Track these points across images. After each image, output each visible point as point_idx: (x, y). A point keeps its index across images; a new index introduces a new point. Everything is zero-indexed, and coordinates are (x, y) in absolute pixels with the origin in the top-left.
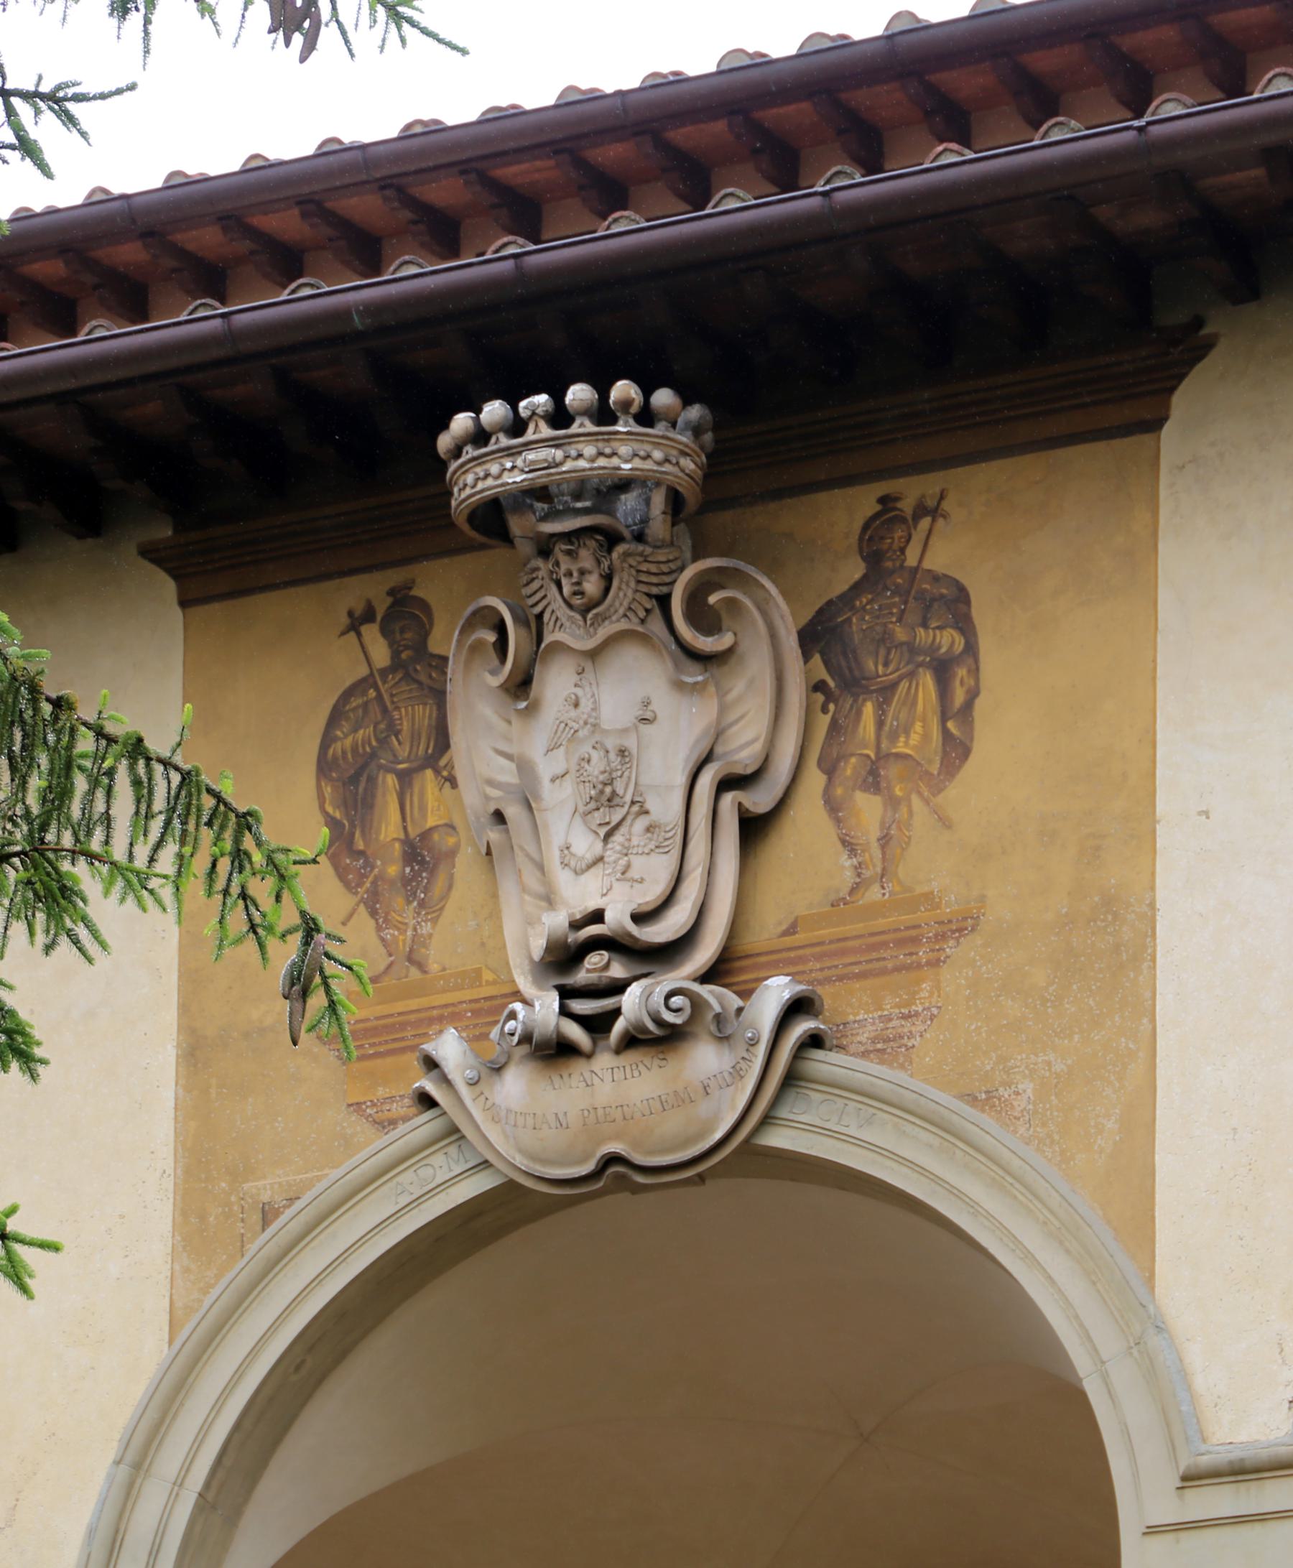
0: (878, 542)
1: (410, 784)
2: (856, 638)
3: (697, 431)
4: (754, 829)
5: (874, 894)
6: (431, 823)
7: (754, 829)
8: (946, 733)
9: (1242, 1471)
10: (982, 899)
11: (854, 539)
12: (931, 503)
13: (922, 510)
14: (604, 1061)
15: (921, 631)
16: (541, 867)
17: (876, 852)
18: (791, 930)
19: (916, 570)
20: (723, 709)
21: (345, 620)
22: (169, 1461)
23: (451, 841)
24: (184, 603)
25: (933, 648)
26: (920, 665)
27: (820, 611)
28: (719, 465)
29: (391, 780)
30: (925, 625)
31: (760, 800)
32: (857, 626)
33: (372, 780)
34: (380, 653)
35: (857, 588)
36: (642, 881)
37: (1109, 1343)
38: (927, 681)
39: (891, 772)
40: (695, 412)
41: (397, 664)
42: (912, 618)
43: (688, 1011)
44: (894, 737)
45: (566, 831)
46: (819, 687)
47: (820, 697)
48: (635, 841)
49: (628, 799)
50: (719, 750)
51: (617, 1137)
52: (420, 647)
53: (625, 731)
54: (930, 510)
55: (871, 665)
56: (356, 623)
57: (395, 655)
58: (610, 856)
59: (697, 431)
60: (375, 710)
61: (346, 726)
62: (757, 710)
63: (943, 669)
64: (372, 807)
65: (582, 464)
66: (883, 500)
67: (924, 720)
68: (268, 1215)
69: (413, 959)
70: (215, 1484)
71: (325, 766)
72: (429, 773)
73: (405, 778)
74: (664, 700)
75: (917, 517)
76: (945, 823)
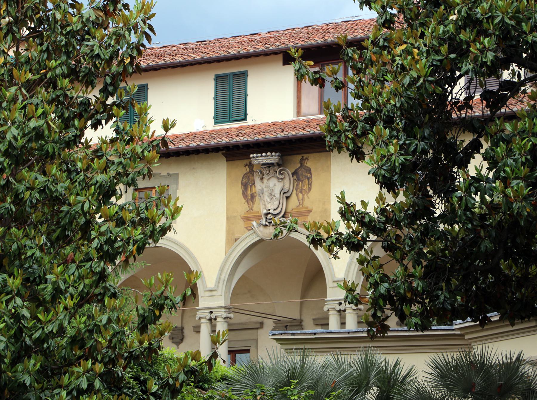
0: (302, 161)
3: (278, 156)
4: (287, 198)
5: (301, 206)
7: (287, 198)
9: (211, 291)
14: (271, 227)
22: (225, 270)
24: (227, 161)
28: (281, 157)
31: (288, 195)
32: (299, 172)
34: (248, 170)
35: (299, 168)
38: (307, 180)
39: (303, 191)
40: (277, 154)
41: (250, 171)
45: (266, 198)
54: (307, 159)
56: (246, 165)
59: (278, 156)
62: (288, 184)
63: (308, 179)
68: (236, 240)
69: (252, 209)
71: (242, 183)
73: (251, 186)
74: (277, 183)
76: (309, 198)
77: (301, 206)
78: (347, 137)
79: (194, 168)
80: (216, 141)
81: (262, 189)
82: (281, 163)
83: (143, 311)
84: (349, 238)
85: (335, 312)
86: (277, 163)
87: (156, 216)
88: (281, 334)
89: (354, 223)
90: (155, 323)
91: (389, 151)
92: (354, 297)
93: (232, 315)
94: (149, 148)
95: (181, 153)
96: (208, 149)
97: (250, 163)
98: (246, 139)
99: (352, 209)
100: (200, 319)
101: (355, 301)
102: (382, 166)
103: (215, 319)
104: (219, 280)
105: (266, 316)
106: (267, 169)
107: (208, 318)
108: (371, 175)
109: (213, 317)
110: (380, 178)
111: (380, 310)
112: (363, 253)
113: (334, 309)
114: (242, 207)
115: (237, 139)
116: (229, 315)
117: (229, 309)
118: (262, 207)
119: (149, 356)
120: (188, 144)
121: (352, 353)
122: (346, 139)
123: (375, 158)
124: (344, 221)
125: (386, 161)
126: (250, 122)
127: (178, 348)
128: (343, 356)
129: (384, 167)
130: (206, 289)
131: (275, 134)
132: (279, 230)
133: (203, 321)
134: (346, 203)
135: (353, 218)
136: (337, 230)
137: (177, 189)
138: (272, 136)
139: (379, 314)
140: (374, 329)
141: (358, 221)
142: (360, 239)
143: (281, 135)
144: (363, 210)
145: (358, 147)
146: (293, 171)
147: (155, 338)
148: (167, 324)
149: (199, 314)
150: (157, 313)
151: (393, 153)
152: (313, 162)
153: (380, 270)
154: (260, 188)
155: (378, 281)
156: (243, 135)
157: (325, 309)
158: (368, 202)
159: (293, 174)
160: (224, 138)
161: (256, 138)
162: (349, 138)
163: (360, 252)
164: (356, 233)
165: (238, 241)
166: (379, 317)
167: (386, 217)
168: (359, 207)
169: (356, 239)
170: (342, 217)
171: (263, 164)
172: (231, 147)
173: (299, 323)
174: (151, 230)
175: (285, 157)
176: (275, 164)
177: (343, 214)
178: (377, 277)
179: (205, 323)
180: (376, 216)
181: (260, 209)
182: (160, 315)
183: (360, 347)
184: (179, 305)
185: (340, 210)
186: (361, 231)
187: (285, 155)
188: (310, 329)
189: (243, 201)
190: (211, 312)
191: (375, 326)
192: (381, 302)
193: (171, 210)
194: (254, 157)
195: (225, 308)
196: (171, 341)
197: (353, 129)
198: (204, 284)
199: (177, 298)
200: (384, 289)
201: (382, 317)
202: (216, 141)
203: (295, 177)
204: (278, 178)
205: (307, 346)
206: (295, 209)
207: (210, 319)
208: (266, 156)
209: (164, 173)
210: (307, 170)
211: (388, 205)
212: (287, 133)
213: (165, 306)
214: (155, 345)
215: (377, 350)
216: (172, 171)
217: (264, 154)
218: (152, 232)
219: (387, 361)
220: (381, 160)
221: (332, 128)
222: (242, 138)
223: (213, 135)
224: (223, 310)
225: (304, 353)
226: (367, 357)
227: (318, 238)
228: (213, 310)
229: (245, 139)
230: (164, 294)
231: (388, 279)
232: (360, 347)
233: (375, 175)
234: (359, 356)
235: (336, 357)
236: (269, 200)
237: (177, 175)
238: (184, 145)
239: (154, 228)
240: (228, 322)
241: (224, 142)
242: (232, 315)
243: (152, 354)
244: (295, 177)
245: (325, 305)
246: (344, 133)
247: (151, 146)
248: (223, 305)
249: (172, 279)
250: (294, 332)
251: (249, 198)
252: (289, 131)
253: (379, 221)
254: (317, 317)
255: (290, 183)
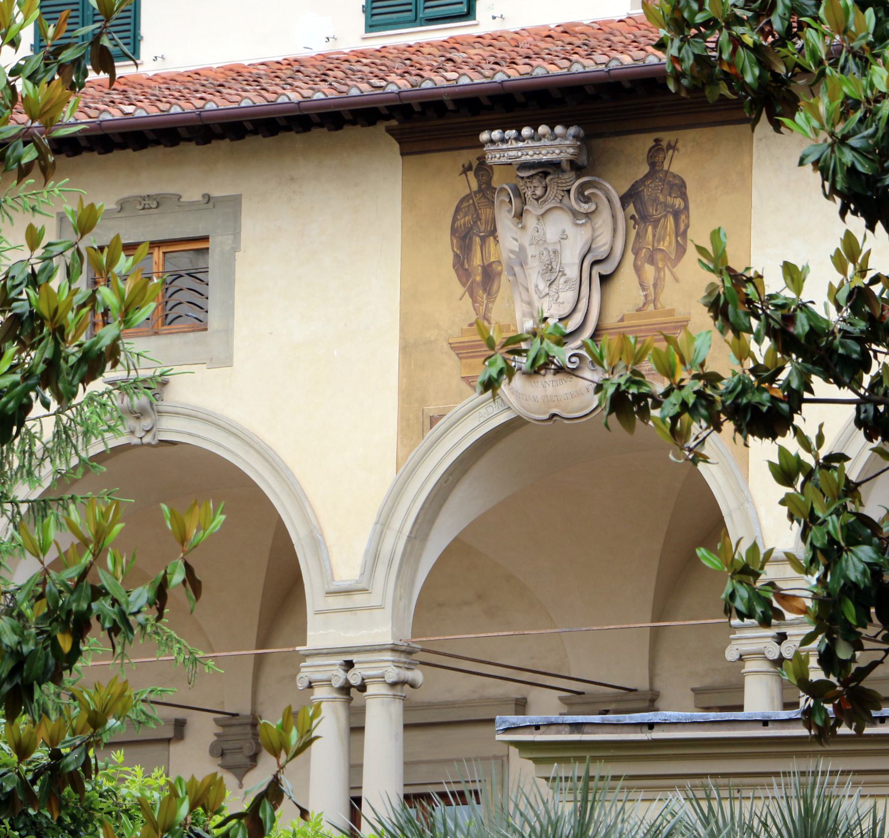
0: (656, 153)
1: (485, 242)
2: (646, 198)
3: (575, 137)
4: (605, 279)
5: (651, 307)
6: (492, 260)
7: (605, 279)
8: (677, 241)
9: (347, 592)
10: (690, 314)
11: (645, 156)
12: (673, 144)
13: (670, 147)
15: (669, 198)
16: (527, 290)
17: (652, 289)
18: (622, 320)
19: (667, 172)
20: (594, 230)
21: (461, 169)
22: (396, 523)
23: (500, 268)
25: (673, 206)
26: (668, 212)
27: (633, 186)
29: (478, 240)
30: (670, 195)
31: (606, 269)
32: (647, 192)
33: (471, 239)
34: (474, 185)
35: (646, 177)
36: (563, 303)
37: (733, 504)
38: (671, 219)
39: (659, 256)
40: (572, 130)
41: (480, 190)
42: (666, 192)
43: (578, 362)
44: (659, 242)
45: (535, 279)
46: (633, 217)
47: (632, 222)
48: (561, 287)
49: (558, 270)
50: (593, 246)
51: (556, 406)
52: (489, 184)
53: (555, 243)
54: (672, 147)
55: (651, 210)
56: (467, 169)
57: (480, 186)
58: (551, 294)
59: (575, 137)
60: (472, 207)
61: (462, 214)
62: (606, 231)
63: (676, 214)
64: (470, 250)
65: (528, 157)
66: (656, 140)
67: (670, 236)
68: (433, 421)
70: (414, 531)
71: (454, 231)
72: (492, 238)
73: (483, 240)
74: (570, 230)
75: (668, 150)
76: (677, 280)
77: (651, 307)
78: (737, 42)
79: (292, 179)
80: (365, 87)
81: (522, 248)
82: (583, 160)
83: (16, 638)
84: (743, 393)
85: (765, 666)
86: (572, 162)
87: (69, 306)
88: (537, 727)
89: (758, 341)
90: (57, 679)
91: (872, 86)
92: (756, 596)
93: (417, 675)
94: (46, 72)
95: (249, 126)
96: (338, 113)
97: (482, 160)
98: (467, 79)
99: (750, 290)
100: (310, 686)
101: (759, 610)
102: (845, 138)
103: (362, 688)
104: (373, 558)
105: (537, 677)
106: (536, 182)
107: (337, 683)
108: (809, 167)
109: (355, 680)
110: (839, 177)
111: (846, 640)
112: (789, 442)
113: (760, 655)
114: (451, 310)
115: (437, 81)
116: (409, 675)
117: (409, 653)
118: (519, 309)
119: (52, 795)
120: (271, 97)
121: (760, 793)
122: (734, 52)
123: (822, 109)
124: (722, 332)
125: (861, 121)
126: (484, 23)
127: (241, 786)
128: (726, 804)
129: (854, 142)
130: (332, 588)
131: (566, 63)
132: (500, 364)
133: (320, 693)
134: (729, 269)
135: (755, 323)
136: (702, 365)
137: (236, 248)
138: (553, 69)
139: (843, 653)
140: (829, 707)
141: (771, 332)
142: (779, 394)
143: (583, 66)
144: (790, 294)
145: (776, 76)
146: (625, 189)
147: (74, 733)
148: (116, 689)
149: (307, 672)
150: (65, 643)
151: (884, 89)
152: (691, 158)
153: (848, 501)
154: (515, 246)
155: (839, 537)
156: (457, 67)
157: (731, 654)
158: (806, 268)
159: (625, 200)
160: (393, 77)
161: (500, 77)
162: (745, 46)
163: (780, 440)
164: (766, 374)
165: (441, 425)
166: (845, 664)
167: (870, 319)
168: (775, 284)
169: (765, 396)
170: (715, 318)
171: (525, 166)
172: (417, 109)
173: (646, 704)
174: (48, 354)
175: (599, 143)
176: (565, 166)
177: (718, 308)
178: (834, 524)
179: (333, 700)
180: (833, 316)
181: (514, 318)
182: (76, 653)
183: (776, 774)
184: (141, 618)
185: (710, 294)
186: (781, 369)
187: (600, 135)
188: (678, 716)
189: (459, 289)
190: (349, 665)
191: (830, 693)
192: (850, 611)
193: (120, 294)
194: (492, 142)
195: (394, 649)
196: (219, 761)
197: (757, 16)
198: (326, 570)
199: (135, 594)
200: (861, 566)
201: (854, 667)
202: (365, 87)
203: (631, 210)
204: (575, 214)
205: (597, 769)
206: (631, 317)
207: (346, 689)
208: (532, 138)
209: (192, 194)
210: (671, 186)
211: (876, 280)
212: (604, 59)
213: (93, 621)
214: (72, 761)
215: (841, 784)
216: (221, 186)
217: (526, 131)
218: (52, 365)
219: (880, 816)
220: (844, 116)
221: (686, 15)
222: (454, 76)
223: (358, 67)
224: (388, 656)
225: (586, 790)
226: (808, 808)
227: (633, 390)
228: (354, 658)
229: (464, 80)
230: (89, 580)
231: (874, 534)
232: (776, 774)
233: (821, 166)
234: (783, 803)
235: (704, 805)
236: (542, 286)
237: (235, 202)
238: (259, 101)
239: (57, 352)
240: (404, 698)
241: (392, 88)
242: (417, 675)
243: (60, 791)
244: (631, 210)
245: (729, 641)
246: (728, 27)
247: (55, 67)
248: (388, 640)
249: (118, 527)
250: (580, 719)
251: (478, 278)
252: (614, 54)
253: (846, 334)
254: (707, 682)
255: (615, 230)
